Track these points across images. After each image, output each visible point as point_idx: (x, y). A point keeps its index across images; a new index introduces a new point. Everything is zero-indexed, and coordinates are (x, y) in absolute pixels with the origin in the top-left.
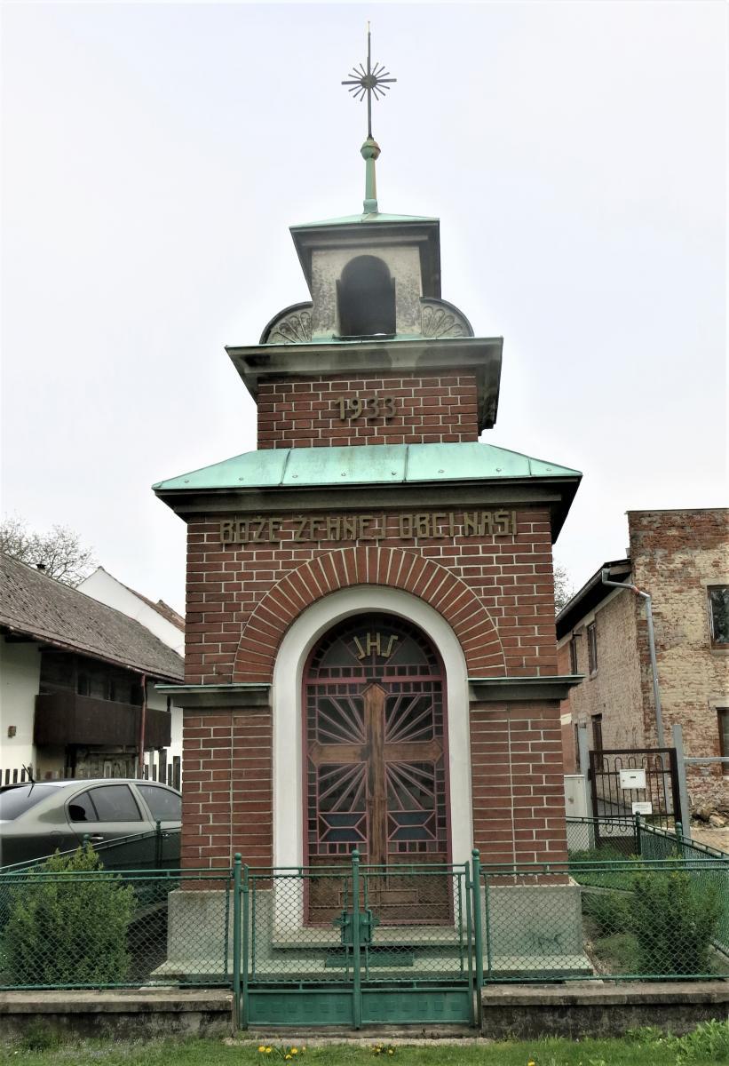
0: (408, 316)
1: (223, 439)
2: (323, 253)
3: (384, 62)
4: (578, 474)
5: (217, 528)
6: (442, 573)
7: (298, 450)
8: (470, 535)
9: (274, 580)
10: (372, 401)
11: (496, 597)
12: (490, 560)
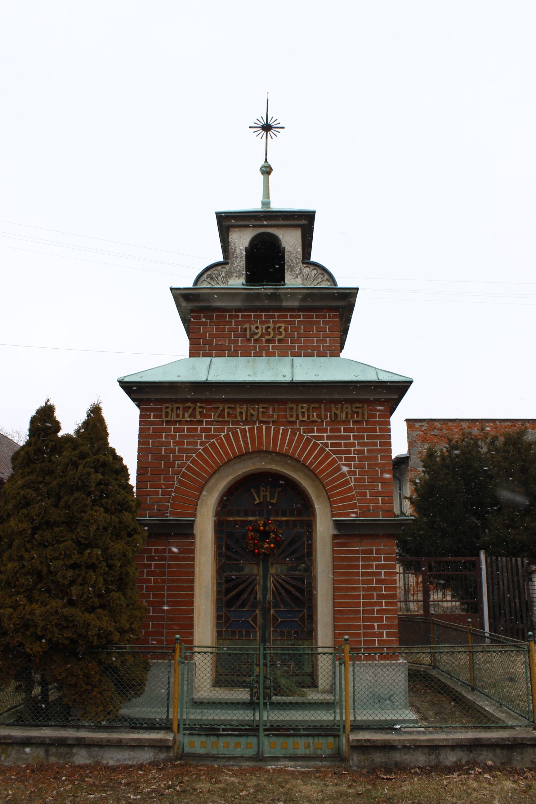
0: (293, 272)
1: (166, 349)
2: (237, 229)
3: (275, 116)
4: (410, 380)
5: (161, 410)
6: (316, 445)
7: (216, 358)
8: (335, 421)
9: (199, 447)
10: (269, 327)
11: (352, 463)
12: (348, 438)
